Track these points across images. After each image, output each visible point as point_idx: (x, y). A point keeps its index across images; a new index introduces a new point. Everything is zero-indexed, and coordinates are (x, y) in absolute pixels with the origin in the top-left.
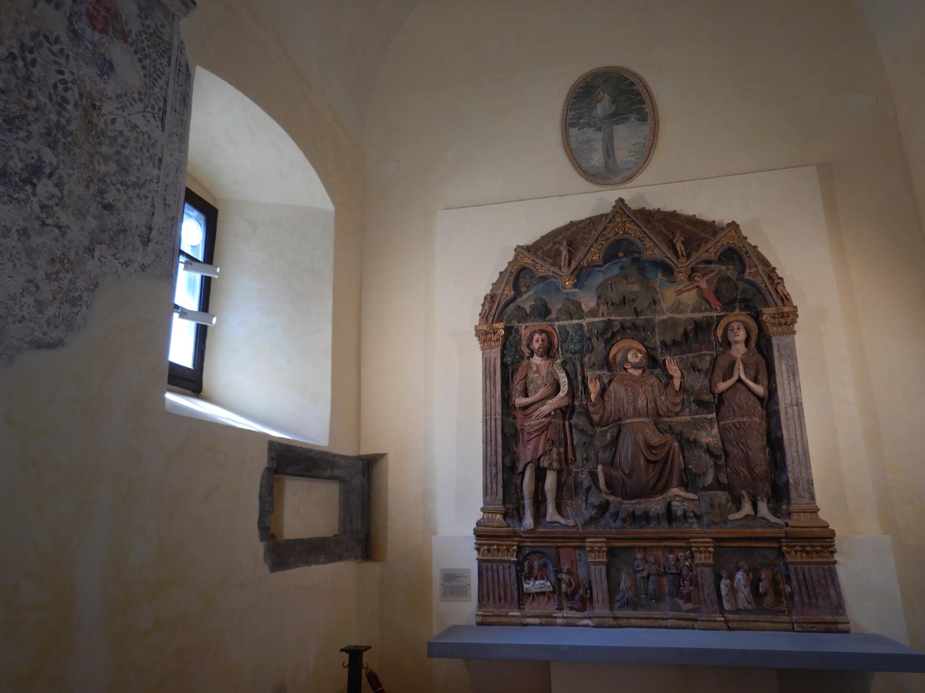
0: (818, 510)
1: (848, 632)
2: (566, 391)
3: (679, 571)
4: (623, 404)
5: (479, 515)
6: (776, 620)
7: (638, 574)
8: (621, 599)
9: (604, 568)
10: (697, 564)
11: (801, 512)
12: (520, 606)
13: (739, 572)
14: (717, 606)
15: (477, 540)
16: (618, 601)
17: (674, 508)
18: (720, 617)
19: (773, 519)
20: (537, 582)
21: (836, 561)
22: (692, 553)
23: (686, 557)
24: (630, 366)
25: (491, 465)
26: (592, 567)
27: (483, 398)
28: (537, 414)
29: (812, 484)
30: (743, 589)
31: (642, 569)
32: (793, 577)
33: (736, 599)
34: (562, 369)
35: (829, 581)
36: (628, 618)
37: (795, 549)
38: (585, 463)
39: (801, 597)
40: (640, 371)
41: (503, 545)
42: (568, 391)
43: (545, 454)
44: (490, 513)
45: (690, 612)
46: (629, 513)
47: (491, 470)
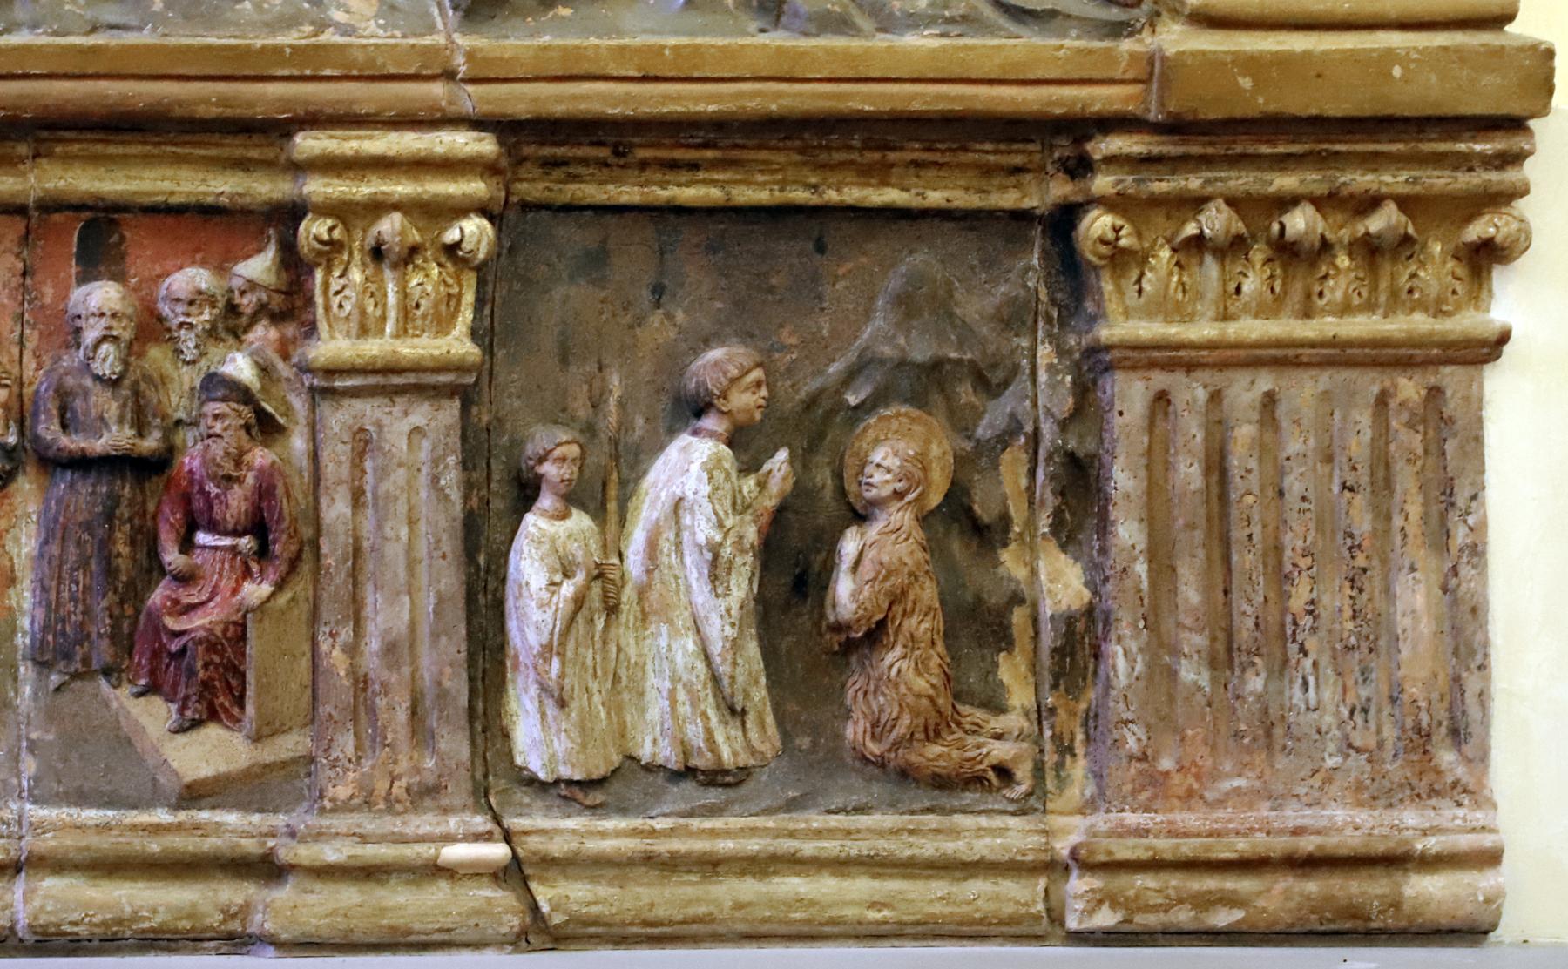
3: (151, 443)
6: (928, 848)
10: (331, 372)
13: (684, 439)
14: (455, 744)
18: (478, 837)
21: (1504, 338)
22: (294, 265)
23: (232, 309)
30: (701, 593)
32: (1123, 479)
35: (1412, 508)
37: (1191, 229)
39: (1161, 650)
45: (715, 159)
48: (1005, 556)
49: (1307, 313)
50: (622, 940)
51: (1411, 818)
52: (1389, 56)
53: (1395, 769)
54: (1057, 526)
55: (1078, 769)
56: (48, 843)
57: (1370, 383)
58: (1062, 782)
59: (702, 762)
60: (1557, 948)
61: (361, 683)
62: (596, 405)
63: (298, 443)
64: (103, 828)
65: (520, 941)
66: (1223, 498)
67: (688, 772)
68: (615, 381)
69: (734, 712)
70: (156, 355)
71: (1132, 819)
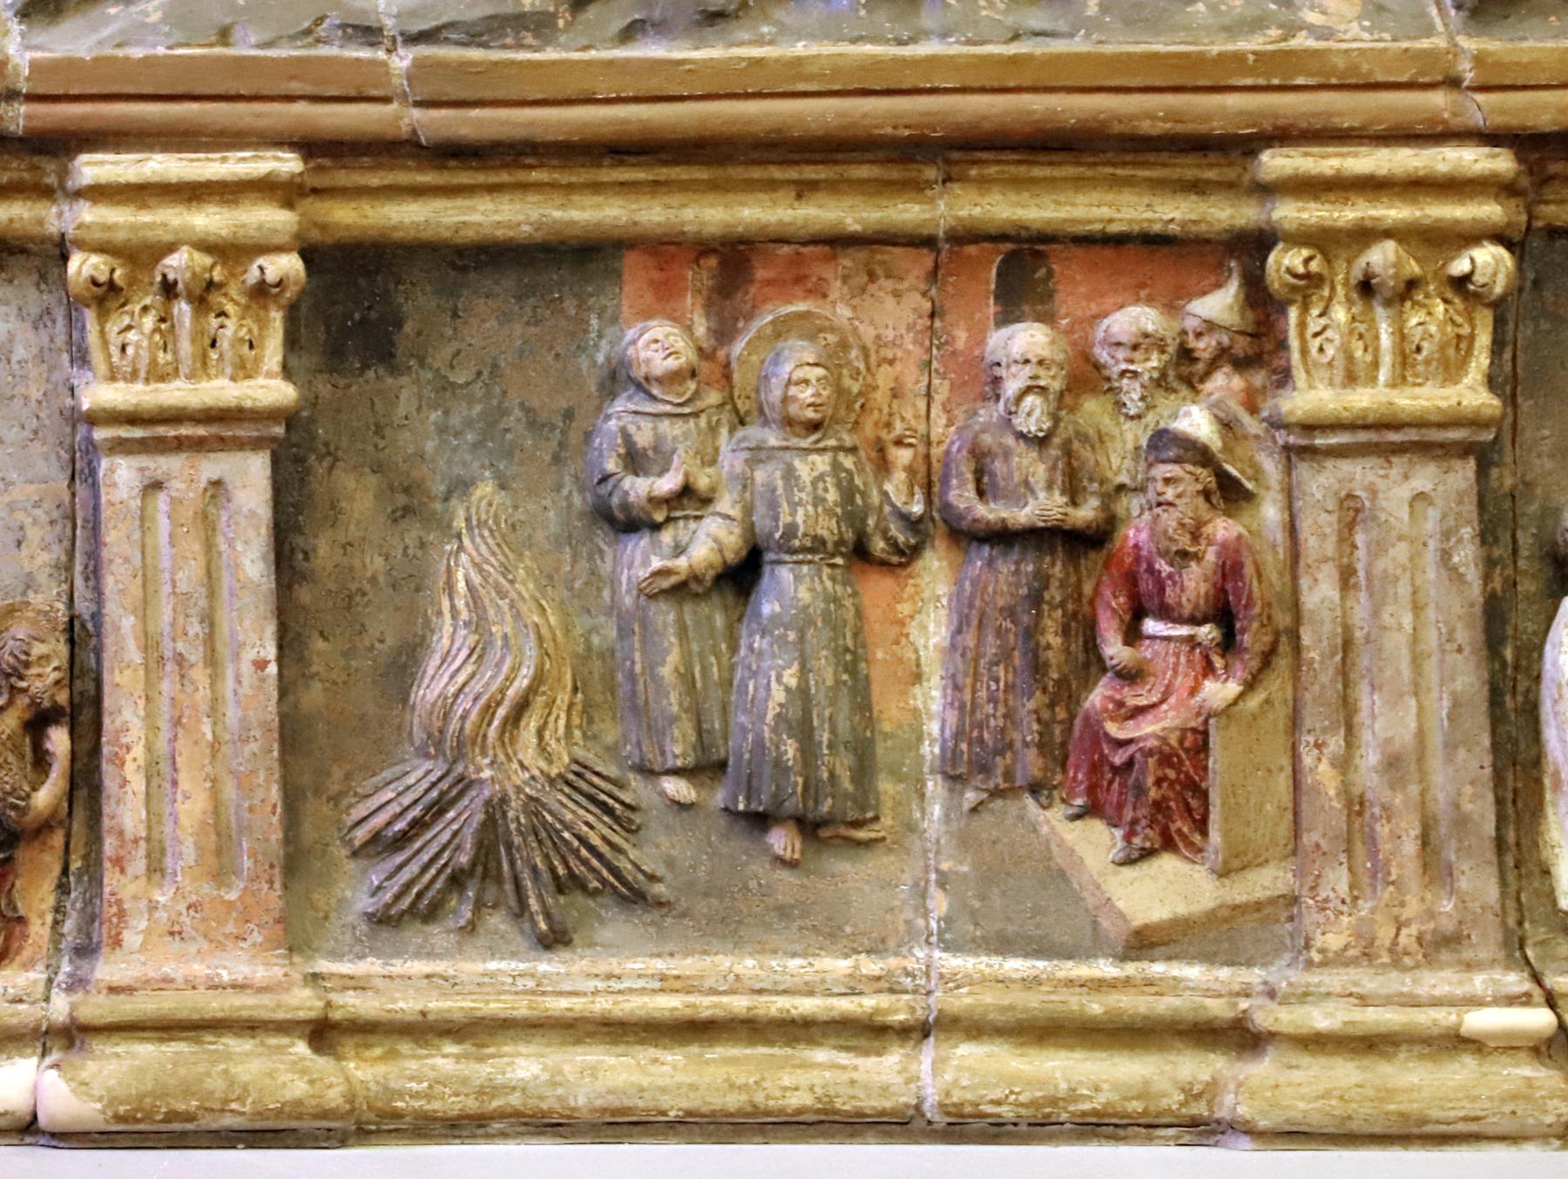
3: (1086, 513)
7: (638, 545)
8: (419, 825)
10: (1309, 427)
16: (382, 845)
18: (1512, 1000)
23: (1186, 354)
31: (686, 492)
56: (962, 1001)
61: (1356, 805)
63: (1271, 512)
70: (1093, 409)
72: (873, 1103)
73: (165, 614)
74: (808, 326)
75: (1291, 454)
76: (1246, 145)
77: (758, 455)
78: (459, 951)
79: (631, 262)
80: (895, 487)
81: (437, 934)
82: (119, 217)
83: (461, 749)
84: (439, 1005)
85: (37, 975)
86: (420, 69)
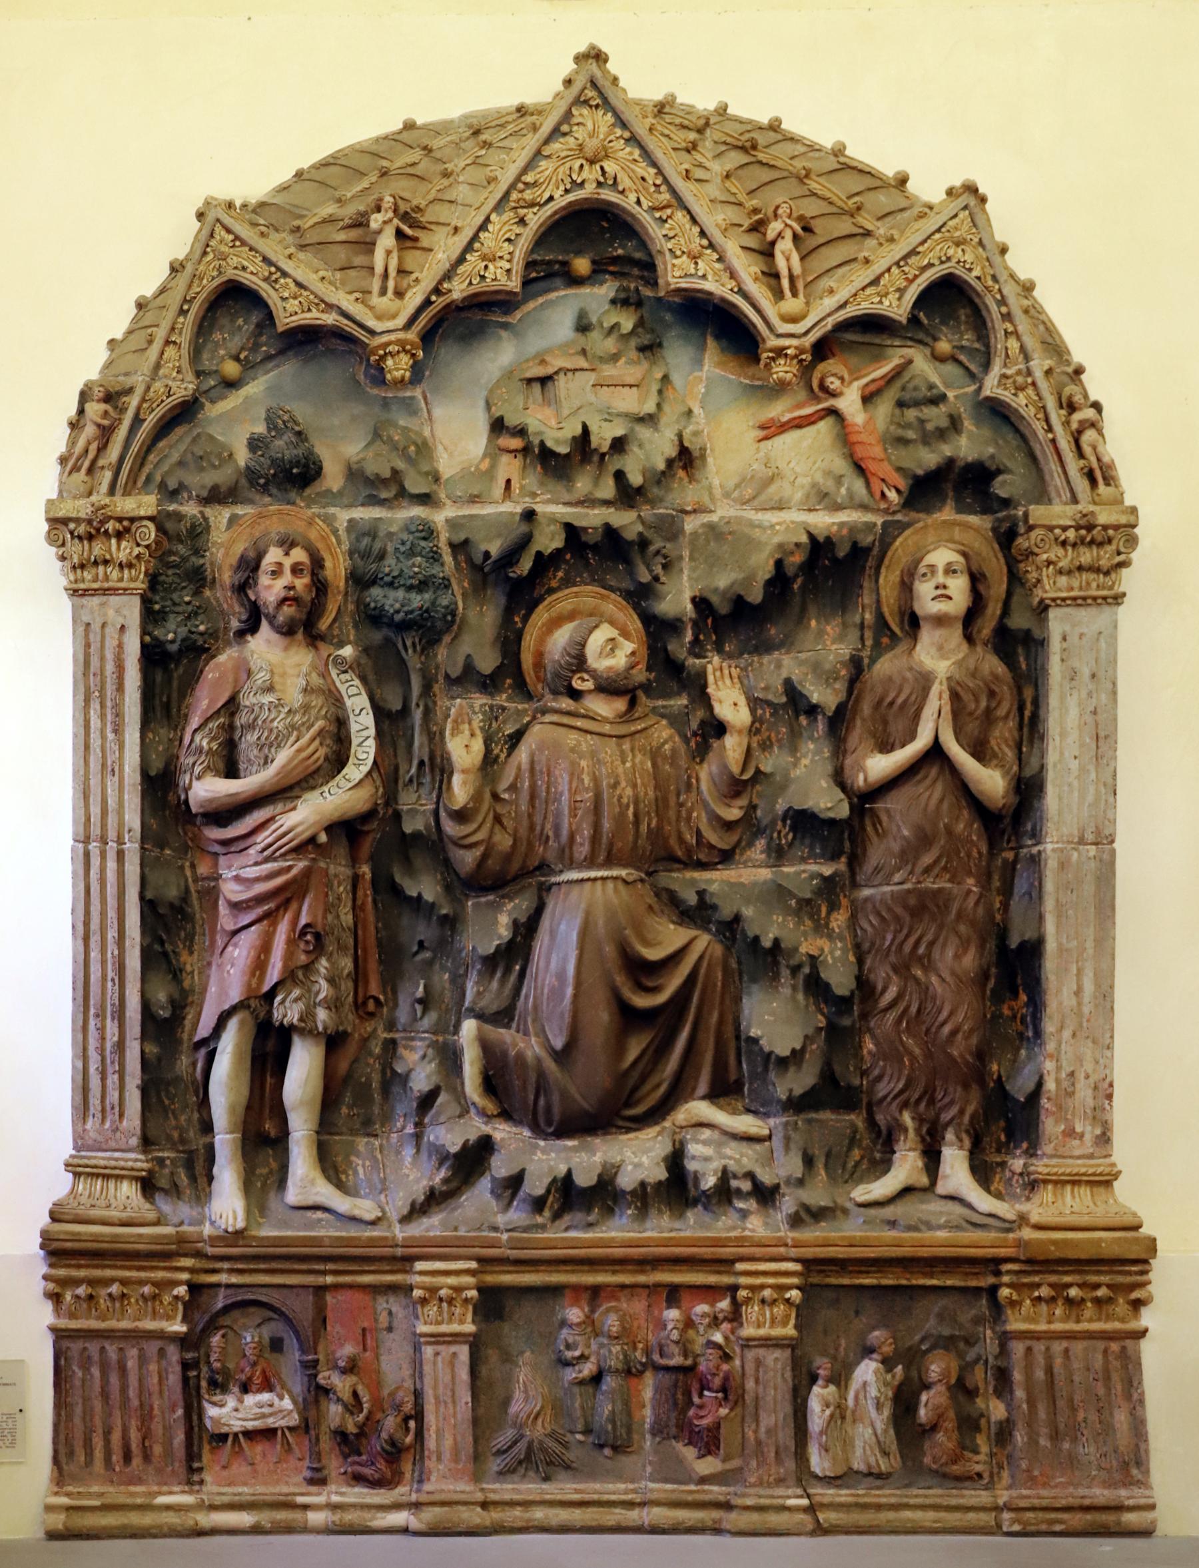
0: (1117, 1175)
1: (1146, 1533)
2: (370, 762)
3: (689, 1362)
4: (558, 815)
5: (60, 1185)
6: (953, 1502)
7: (569, 1370)
8: (510, 1447)
9: (464, 1352)
10: (748, 1339)
11: (1068, 1182)
12: (192, 1473)
13: (866, 1361)
14: (790, 1464)
15: (51, 1266)
16: (500, 1452)
17: (691, 1166)
19: (983, 1201)
20: (250, 1400)
21: (1146, 1330)
22: (736, 1305)
23: (716, 1318)
24: (589, 685)
25: (101, 1015)
26: (428, 1351)
27: (75, 773)
28: (270, 840)
29: (1110, 1097)
32: (1017, 1376)
33: (847, 1444)
34: (357, 682)
35: (1118, 1387)
36: (526, 1504)
37: (1036, 1294)
38: (419, 1014)
40: (620, 705)
41: (142, 1283)
42: (375, 762)
43: (289, 978)
44: (97, 1175)
46: (554, 1180)
47: (102, 1030)
48: (978, 1400)
49: (1078, 1321)
50: (848, 1532)
51: (1123, 1493)
52: (1100, 1240)
53: (1117, 1476)
54: (995, 1391)
55: (1005, 1474)
56: (654, 1496)
57: (1101, 1345)
58: (1000, 1478)
59: (875, 1471)
60: (1190, 1540)
61: (759, 1443)
62: (837, 1349)
63: (737, 1362)
64: (673, 1491)
65: (813, 1533)
66: (1052, 1382)
67: (870, 1474)
68: (843, 1342)
69: (886, 1454)
70: (691, 1333)
71: (1025, 1492)
72: (631, 1524)
73: (441, 1390)
74: (616, 1310)
75: (743, 1347)
76: (732, 1262)
77: (602, 1346)
78: (521, 1482)
79: (567, 1291)
80: (638, 1354)
81: (516, 1477)
82: (427, 1279)
83: (521, 1427)
84: (516, 1497)
85: (407, 1488)
86: (510, 1238)
